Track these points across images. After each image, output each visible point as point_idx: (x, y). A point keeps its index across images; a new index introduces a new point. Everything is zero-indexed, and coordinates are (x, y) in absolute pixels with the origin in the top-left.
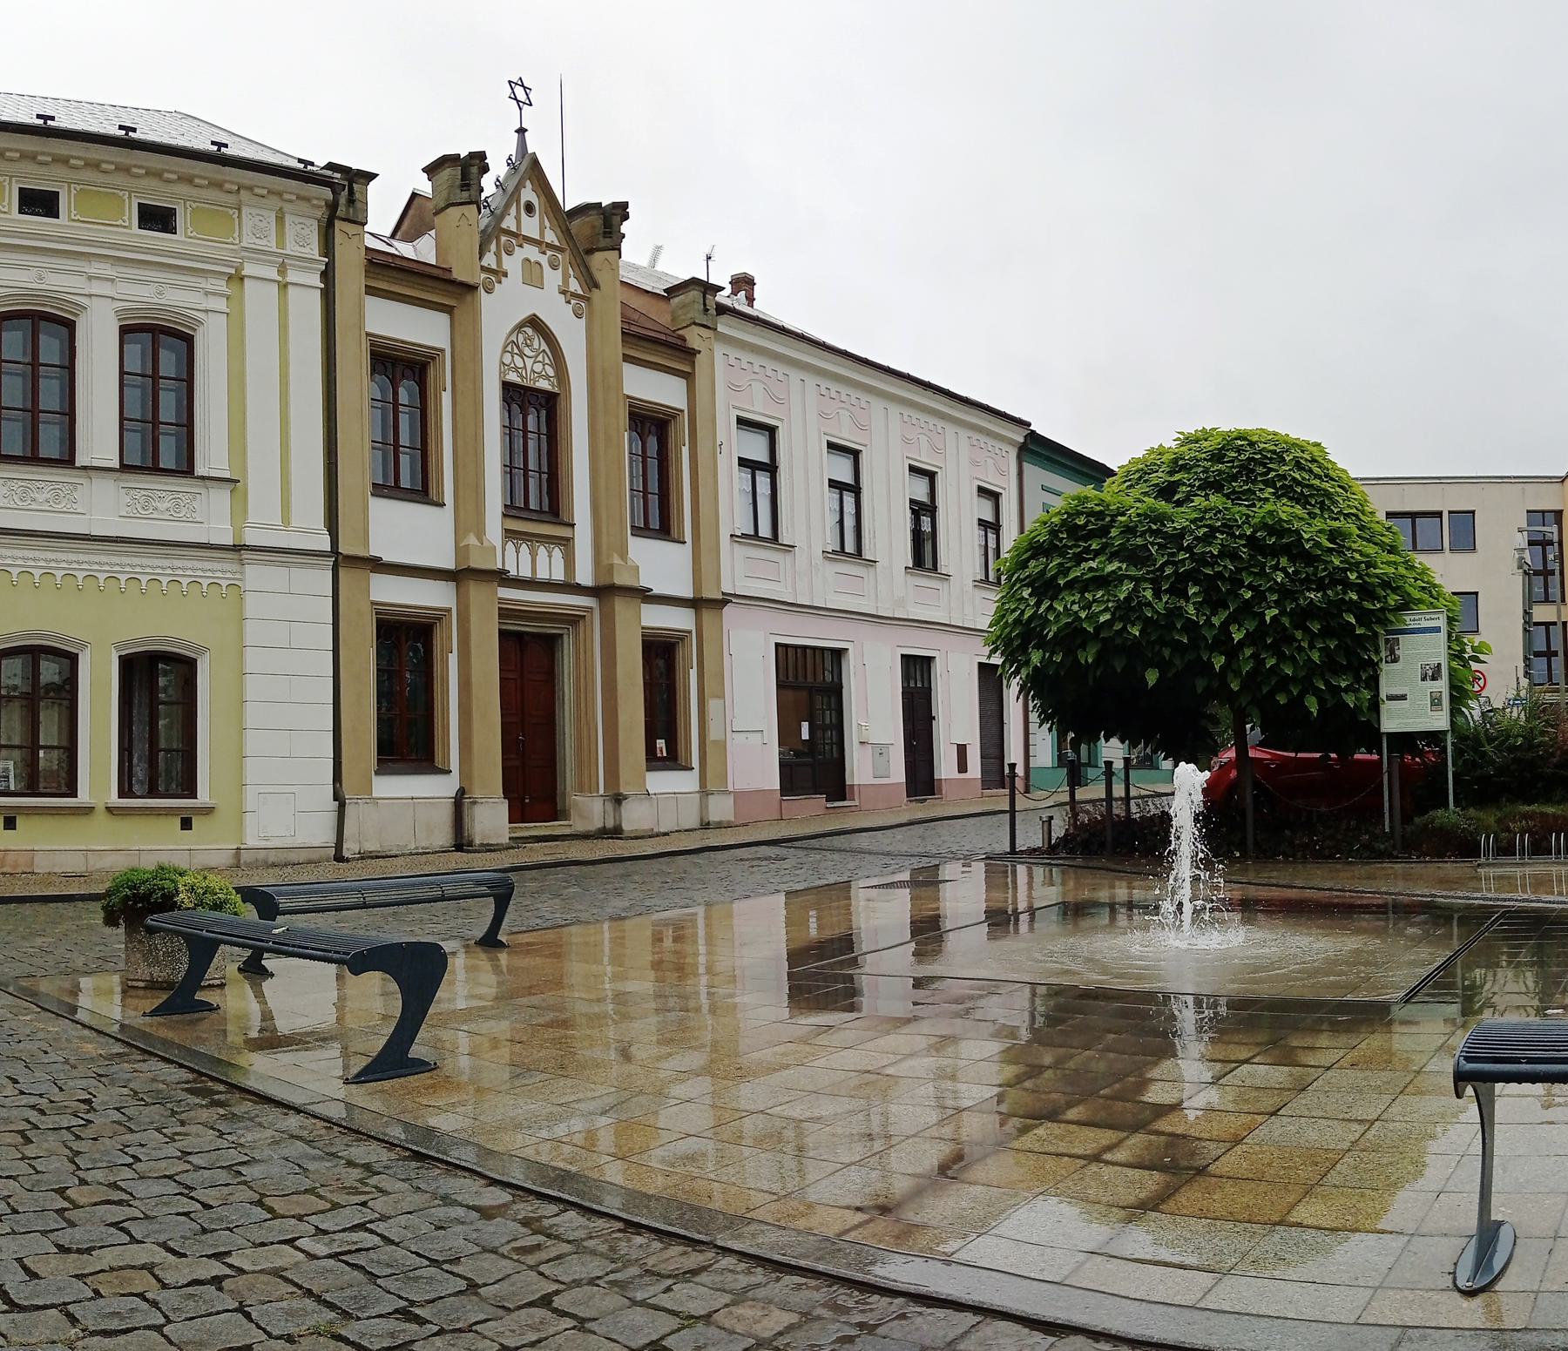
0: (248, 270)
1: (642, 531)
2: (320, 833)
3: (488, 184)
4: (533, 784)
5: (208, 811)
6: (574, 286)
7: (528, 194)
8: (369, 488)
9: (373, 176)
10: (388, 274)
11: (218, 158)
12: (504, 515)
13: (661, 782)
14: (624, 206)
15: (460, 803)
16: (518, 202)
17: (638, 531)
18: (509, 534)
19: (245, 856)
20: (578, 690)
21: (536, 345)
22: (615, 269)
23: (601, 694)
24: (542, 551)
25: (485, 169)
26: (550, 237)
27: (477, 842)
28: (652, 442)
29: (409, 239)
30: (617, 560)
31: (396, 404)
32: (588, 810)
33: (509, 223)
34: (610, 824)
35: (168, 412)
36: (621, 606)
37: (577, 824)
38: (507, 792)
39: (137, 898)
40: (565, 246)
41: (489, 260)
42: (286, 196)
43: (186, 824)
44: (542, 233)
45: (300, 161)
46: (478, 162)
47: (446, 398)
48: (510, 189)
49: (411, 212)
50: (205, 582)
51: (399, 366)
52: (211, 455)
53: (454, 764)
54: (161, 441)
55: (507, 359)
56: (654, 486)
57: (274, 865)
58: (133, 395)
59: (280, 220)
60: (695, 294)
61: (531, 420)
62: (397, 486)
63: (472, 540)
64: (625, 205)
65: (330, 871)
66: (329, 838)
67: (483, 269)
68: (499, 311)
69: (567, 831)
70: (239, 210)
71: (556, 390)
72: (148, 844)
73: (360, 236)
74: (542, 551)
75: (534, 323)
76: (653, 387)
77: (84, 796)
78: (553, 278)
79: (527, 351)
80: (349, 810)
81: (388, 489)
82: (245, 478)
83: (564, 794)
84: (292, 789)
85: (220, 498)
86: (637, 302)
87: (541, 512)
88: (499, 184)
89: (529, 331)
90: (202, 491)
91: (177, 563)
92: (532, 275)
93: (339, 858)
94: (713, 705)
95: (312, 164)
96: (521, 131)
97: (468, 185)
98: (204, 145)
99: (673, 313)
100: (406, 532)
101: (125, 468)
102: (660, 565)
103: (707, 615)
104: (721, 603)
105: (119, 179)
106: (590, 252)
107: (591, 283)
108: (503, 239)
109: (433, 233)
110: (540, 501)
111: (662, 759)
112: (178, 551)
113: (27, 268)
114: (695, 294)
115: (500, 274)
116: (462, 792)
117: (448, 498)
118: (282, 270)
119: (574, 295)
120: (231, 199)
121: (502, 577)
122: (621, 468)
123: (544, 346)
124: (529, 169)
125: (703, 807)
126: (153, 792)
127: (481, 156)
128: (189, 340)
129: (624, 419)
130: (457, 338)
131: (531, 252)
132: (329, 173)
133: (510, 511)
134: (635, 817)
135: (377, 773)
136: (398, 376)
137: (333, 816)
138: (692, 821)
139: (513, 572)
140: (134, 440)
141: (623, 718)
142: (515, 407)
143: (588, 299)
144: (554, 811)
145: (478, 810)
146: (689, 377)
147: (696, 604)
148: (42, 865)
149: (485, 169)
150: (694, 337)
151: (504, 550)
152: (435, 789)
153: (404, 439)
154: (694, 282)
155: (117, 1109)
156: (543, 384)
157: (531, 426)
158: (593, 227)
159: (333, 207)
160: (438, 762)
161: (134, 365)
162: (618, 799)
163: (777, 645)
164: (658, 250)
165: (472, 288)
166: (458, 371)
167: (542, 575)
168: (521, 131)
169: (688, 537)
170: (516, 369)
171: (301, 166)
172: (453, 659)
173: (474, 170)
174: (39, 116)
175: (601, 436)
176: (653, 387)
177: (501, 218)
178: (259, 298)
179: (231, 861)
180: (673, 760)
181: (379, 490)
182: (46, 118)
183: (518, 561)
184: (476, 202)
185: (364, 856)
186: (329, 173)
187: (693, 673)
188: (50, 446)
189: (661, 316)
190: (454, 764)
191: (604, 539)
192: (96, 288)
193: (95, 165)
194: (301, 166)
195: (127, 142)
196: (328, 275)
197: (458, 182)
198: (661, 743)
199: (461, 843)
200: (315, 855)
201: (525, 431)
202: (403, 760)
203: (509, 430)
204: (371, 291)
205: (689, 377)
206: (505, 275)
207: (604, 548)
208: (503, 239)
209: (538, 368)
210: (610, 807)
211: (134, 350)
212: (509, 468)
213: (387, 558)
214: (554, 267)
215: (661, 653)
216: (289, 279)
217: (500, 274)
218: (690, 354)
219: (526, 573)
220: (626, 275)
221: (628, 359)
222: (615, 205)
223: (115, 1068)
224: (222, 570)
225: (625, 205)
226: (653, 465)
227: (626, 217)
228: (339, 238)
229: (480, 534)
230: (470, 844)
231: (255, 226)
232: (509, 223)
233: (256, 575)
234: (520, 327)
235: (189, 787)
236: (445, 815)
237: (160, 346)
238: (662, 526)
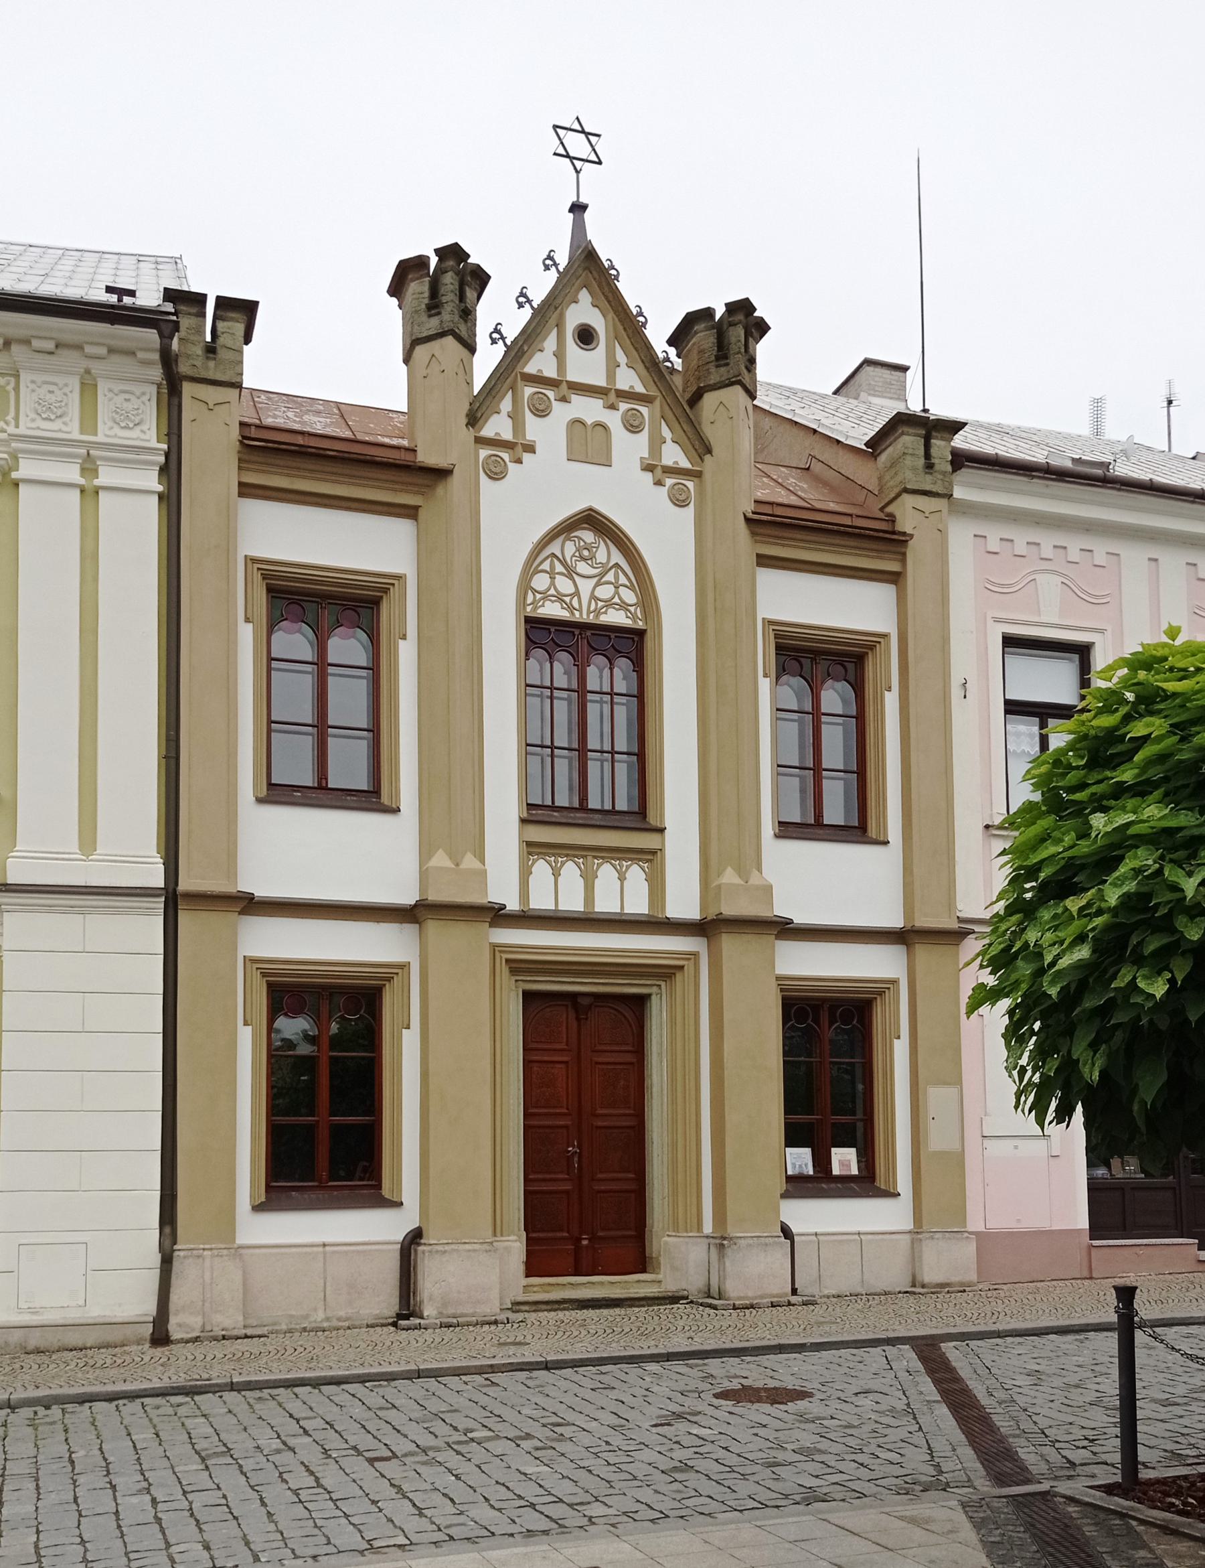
0: (26, 469)
6: (674, 455)
7: (583, 310)
8: (235, 489)
12: (523, 821)
13: (811, 1216)
16: (560, 326)
18: (532, 849)
21: (601, 556)
23: (715, 1083)
24: (606, 873)
33: (541, 363)
37: (666, 1280)
40: (654, 392)
44: (611, 376)
57: (38, 1351)
59: (88, 388)
60: (909, 441)
66: (150, 1307)
68: (513, 512)
71: (640, 625)
78: (630, 449)
89: (588, 536)
93: (160, 1338)
94: (937, 1097)
96: (578, 209)
100: (368, 855)
106: (696, 399)
107: (701, 447)
111: (845, 1179)
116: (416, 1236)
118: (89, 467)
123: (617, 557)
124: (588, 270)
125: (914, 1257)
131: (590, 409)
133: (535, 814)
138: (893, 1275)
143: (696, 475)
156: (615, 617)
158: (701, 352)
162: (721, 1243)
164: (1098, 405)
167: (606, 904)
170: (560, 598)
171: (113, 299)
174: (109, 290)
194: (113, 299)
196: (171, 469)
207: (714, 862)
208: (528, 391)
214: (633, 427)
216: (100, 481)
217: (520, 448)
219: (573, 903)
221: (764, 561)
234: (567, 528)
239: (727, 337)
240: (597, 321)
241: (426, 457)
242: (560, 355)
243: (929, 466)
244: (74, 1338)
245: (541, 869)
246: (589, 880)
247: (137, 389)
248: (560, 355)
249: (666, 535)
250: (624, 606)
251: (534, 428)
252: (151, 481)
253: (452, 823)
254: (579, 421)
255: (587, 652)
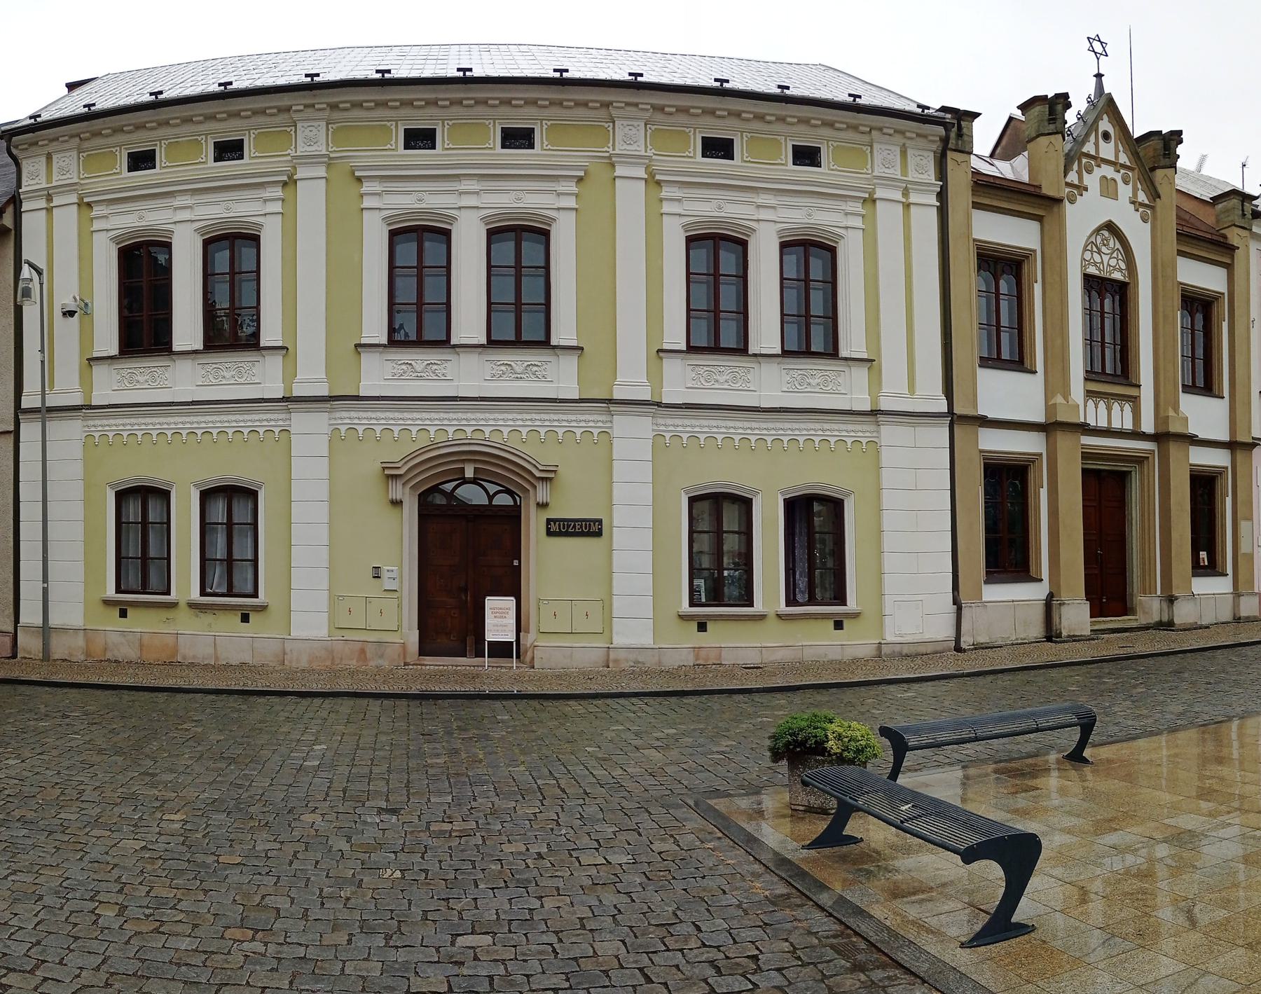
0: (879, 193)
1: (1190, 389)
2: (941, 630)
3: (1071, 117)
4: (1108, 587)
5: (855, 616)
6: (1142, 197)
7: (1105, 125)
8: (977, 361)
9: (977, 115)
10: (990, 192)
11: (853, 107)
12: (1086, 379)
13: (1203, 586)
14: (1178, 134)
15: (1049, 605)
16: (1097, 131)
17: (1188, 389)
18: (1089, 394)
19: (885, 649)
20: (1143, 515)
21: (1111, 244)
22: (1172, 183)
23: (1159, 519)
24: (1116, 407)
25: (1069, 106)
26: (1123, 159)
27: (1064, 633)
28: (1199, 317)
29: (1007, 157)
30: (1171, 413)
31: (997, 294)
32: (1149, 607)
33: (1089, 148)
34: (1165, 619)
35: (817, 308)
36: (1174, 449)
37: (1141, 619)
38: (1089, 595)
39: (797, 743)
41: (1072, 177)
42: (908, 134)
43: (839, 625)
44: (1117, 156)
45: (919, 106)
46: (1062, 100)
47: (1038, 288)
48: (1090, 122)
49: (1008, 132)
50: (849, 441)
51: (1000, 265)
52: (852, 341)
53: (1045, 574)
54: (813, 333)
55: (1088, 255)
56: (1200, 352)
58: (792, 295)
59: (904, 153)
60: (1235, 202)
61: (1107, 302)
62: (999, 358)
63: (1059, 399)
64: (1180, 133)
65: (53, 147)
66: (950, 633)
67: (1068, 184)
68: (1081, 218)
69: (1134, 624)
70: (871, 146)
71: (1127, 280)
72: (814, 642)
73: (968, 162)
74: (1116, 407)
75: (1110, 227)
76: (1202, 276)
77: (759, 606)
78: (1125, 191)
79: (1104, 249)
80: (965, 612)
81: (992, 361)
82: (879, 356)
83: (1132, 595)
84: (920, 597)
85: (860, 375)
86: (1188, 206)
87: (1115, 375)
88: (1080, 117)
89: (1106, 234)
90: (846, 369)
91: (826, 426)
92: (1109, 189)
93: (958, 649)
94: (1243, 525)
95: (928, 108)
96: (1099, 76)
97: (1054, 119)
98: (843, 97)
99: (1217, 216)
100: (1007, 395)
101: (786, 353)
102: (1204, 416)
103: (1240, 455)
104: (1251, 446)
105: (778, 127)
106: (1153, 169)
107: (1155, 194)
108: (1084, 160)
109: (1026, 153)
110: (1114, 369)
111: (1204, 567)
112: (830, 417)
113: (708, 200)
114: (1235, 202)
115: (1081, 188)
116: (1051, 596)
117: (1040, 366)
118: (906, 193)
119: (1142, 205)
120: (866, 138)
121: (1085, 429)
122: (1175, 340)
123: (1118, 246)
124: (1105, 105)
125: (1236, 605)
126: (812, 601)
127: (1065, 96)
128: (832, 251)
129: (1177, 301)
130: (1046, 238)
131: (1108, 171)
132: (941, 114)
133: (1090, 376)
134: (1184, 613)
135: (986, 582)
136: (999, 272)
137: (952, 617)
138: (1226, 615)
139: (1093, 423)
140: (792, 330)
141: (1175, 535)
142: (1094, 293)
143: (1152, 208)
144: (1124, 607)
145: (1064, 609)
146: (1229, 267)
147: (1231, 446)
148: (728, 659)
149: (1068, 106)
150: (1234, 236)
151: (1085, 406)
152: (1030, 593)
153: (1004, 321)
154: (1234, 193)
155: (779, 970)
156: (1117, 276)
157: (1107, 308)
158: (1155, 150)
159: (945, 141)
160: (1033, 573)
161: (791, 273)
162: (1171, 600)
163: (732, 159)
165: (1059, 201)
166: (1047, 267)
167: (1116, 424)
168: (1099, 76)
169: (1226, 393)
170: (1095, 264)
171: (920, 110)
172: (1044, 493)
173: (1059, 107)
175: (1161, 315)
176: (1202, 276)
177: (1083, 143)
178: (888, 216)
179: (874, 653)
180: (1213, 569)
181: (985, 362)
182: (722, 81)
183: (1096, 415)
184: (1061, 132)
185: (978, 647)
186: (941, 114)
187: (1229, 500)
188: (729, 338)
189: (1207, 217)
190: (1045, 574)
191: (1162, 396)
192: (763, 214)
193: (760, 117)
194: (920, 110)
195: (782, 98)
196: (942, 195)
197: (1047, 117)
198: (1203, 555)
199: (1051, 634)
200: (939, 647)
201: (1102, 312)
202: (1005, 571)
203: (1089, 311)
204: (976, 206)
205: (1229, 267)
206: (1086, 189)
207: (1162, 403)
208: (1084, 160)
209: (1113, 262)
210: (1165, 605)
211: (791, 259)
212: (1089, 341)
213: (991, 415)
214: (1126, 183)
215: (1205, 486)
217: (1081, 188)
218: (1231, 249)
219: (1103, 423)
220: (1181, 183)
221: (1181, 253)
222: (1172, 133)
223: (779, 916)
224: (861, 431)
225: (1180, 133)
226: (1200, 336)
227: (1181, 142)
228: (950, 165)
229: (1066, 394)
230: (1059, 635)
231: (885, 159)
232: (1089, 148)
233: (890, 433)
234: (1097, 231)
235: (840, 598)
236: (1038, 615)
237: (811, 257)
238: (1205, 385)
239: (1165, 146)
240: (1111, 131)
241: (1046, 191)
242: (1097, 144)
243: (1244, 215)
244: (922, 649)
245: (1091, 403)
246: (1109, 409)
247: (926, 154)
248: (1097, 144)
249: (1139, 234)
250: (1120, 270)
251: (1088, 180)
252: (933, 200)
253: (1056, 383)
254: (1104, 177)
255: (1109, 294)
